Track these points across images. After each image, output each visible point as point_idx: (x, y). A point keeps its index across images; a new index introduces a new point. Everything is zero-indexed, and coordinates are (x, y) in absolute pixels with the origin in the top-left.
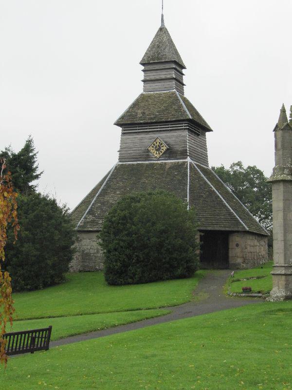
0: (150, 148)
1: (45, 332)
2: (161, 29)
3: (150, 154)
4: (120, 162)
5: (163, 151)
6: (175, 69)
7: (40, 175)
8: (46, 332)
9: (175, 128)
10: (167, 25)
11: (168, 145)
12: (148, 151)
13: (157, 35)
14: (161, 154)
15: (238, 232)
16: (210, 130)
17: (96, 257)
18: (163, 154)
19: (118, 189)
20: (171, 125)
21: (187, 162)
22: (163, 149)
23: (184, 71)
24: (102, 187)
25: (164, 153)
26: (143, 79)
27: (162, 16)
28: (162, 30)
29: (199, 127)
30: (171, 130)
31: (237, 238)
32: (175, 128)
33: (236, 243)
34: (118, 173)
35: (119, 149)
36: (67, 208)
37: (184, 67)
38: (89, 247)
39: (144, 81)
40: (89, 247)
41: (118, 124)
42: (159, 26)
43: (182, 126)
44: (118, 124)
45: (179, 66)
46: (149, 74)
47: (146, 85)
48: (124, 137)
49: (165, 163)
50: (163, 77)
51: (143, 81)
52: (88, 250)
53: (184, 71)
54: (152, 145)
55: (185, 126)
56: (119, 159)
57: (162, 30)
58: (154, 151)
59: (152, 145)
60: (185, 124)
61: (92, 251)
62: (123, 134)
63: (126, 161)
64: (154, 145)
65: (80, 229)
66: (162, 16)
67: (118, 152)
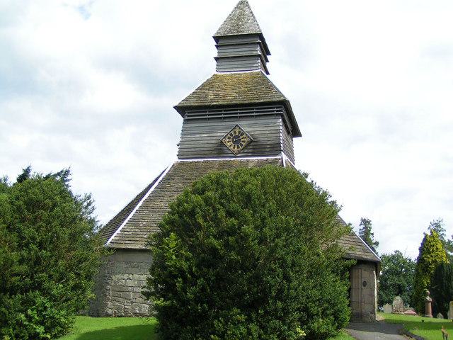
3: (225, 148)
4: (179, 159)
5: (244, 144)
6: (259, 43)
12: (222, 144)
13: (237, 7)
16: (27, 171)
18: (243, 148)
23: (268, 57)
24: (161, 179)
25: (246, 147)
26: (216, 55)
29: (294, 131)
30: (240, 117)
33: (363, 280)
34: (174, 174)
35: (178, 140)
37: (269, 53)
39: (216, 59)
41: (181, 109)
43: (273, 111)
44: (181, 109)
45: (266, 51)
49: (248, 161)
51: (216, 59)
53: (268, 57)
62: (186, 121)
63: (187, 159)
64: (231, 135)
65: (115, 246)
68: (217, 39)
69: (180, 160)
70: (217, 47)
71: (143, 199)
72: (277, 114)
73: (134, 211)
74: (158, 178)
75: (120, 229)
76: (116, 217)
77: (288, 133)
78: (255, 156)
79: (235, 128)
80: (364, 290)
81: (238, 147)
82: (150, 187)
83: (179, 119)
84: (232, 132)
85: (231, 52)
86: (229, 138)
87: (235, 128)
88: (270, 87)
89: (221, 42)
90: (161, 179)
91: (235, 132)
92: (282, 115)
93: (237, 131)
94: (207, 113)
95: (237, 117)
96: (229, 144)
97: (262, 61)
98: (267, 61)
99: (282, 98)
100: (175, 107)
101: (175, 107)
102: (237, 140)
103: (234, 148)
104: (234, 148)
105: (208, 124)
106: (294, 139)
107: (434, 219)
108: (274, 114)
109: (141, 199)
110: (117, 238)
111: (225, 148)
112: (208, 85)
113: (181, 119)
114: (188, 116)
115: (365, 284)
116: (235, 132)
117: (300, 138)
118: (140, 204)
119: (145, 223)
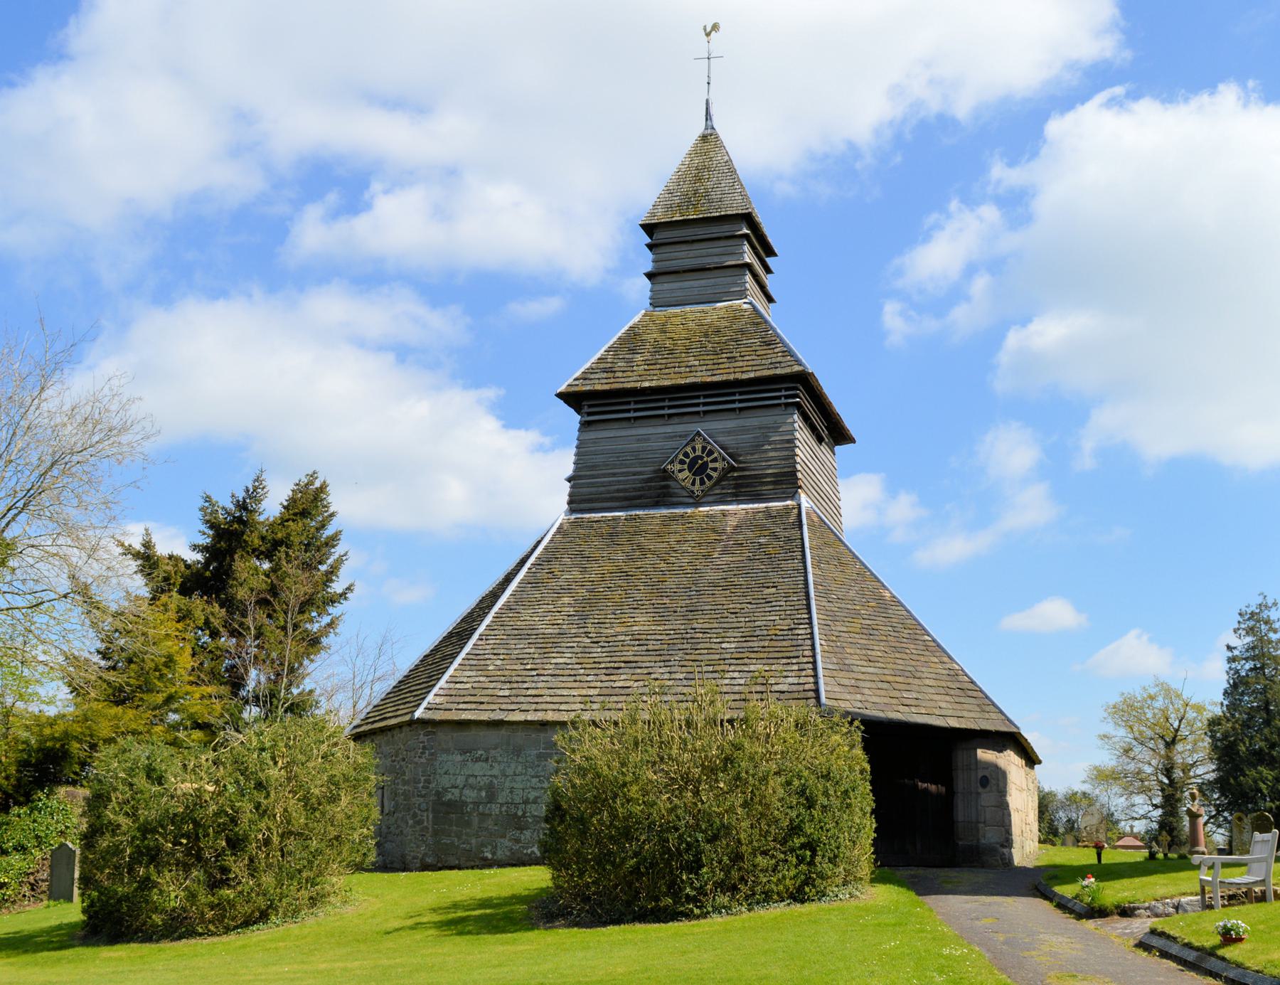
1: (806, 616)
2: (704, 138)
3: (671, 483)
6: (746, 236)
7: (340, 616)
8: (807, 624)
12: (665, 475)
17: (483, 816)
19: (568, 590)
22: (715, 469)
23: (770, 261)
26: (649, 267)
27: (707, 101)
28: (709, 138)
30: (705, 412)
33: (980, 774)
36: (317, 484)
37: (770, 252)
38: (460, 781)
39: (650, 276)
40: (460, 781)
42: (700, 128)
44: (572, 398)
46: (667, 252)
47: (658, 287)
48: (592, 435)
49: (724, 514)
50: (565, 694)
52: (456, 792)
53: (770, 261)
54: (681, 457)
56: (570, 503)
57: (709, 138)
59: (681, 457)
61: (470, 795)
62: (585, 425)
64: (686, 455)
65: (438, 716)
66: (707, 101)
67: (569, 480)
68: (649, 228)
69: (573, 517)
71: (496, 609)
72: (787, 405)
73: (476, 636)
74: (494, 595)
75: (446, 677)
76: (435, 650)
77: (820, 440)
78: (740, 502)
79: (693, 440)
80: (984, 796)
81: (702, 483)
82: (508, 579)
83: (572, 419)
84: (689, 449)
85: (684, 257)
86: (682, 462)
87: (693, 440)
88: (771, 341)
89: (661, 236)
90: (532, 560)
91: (694, 449)
93: (699, 447)
94: (632, 406)
95: (698, 413)
96: (681, 476)
97: (755, 276)
98: (768, 270)
99: (797, 368)
102: (698, 468)
103: (693, 484)
104: (693, 484)
105: (633, 432)
106: (837, 448)
107: (1043, 762)
108: (779, 405)
109: (490, 607)
110: (438, 700)
112: (631, 341)
117: (851, 445)
118: (488, 620)
119: (499, 663)
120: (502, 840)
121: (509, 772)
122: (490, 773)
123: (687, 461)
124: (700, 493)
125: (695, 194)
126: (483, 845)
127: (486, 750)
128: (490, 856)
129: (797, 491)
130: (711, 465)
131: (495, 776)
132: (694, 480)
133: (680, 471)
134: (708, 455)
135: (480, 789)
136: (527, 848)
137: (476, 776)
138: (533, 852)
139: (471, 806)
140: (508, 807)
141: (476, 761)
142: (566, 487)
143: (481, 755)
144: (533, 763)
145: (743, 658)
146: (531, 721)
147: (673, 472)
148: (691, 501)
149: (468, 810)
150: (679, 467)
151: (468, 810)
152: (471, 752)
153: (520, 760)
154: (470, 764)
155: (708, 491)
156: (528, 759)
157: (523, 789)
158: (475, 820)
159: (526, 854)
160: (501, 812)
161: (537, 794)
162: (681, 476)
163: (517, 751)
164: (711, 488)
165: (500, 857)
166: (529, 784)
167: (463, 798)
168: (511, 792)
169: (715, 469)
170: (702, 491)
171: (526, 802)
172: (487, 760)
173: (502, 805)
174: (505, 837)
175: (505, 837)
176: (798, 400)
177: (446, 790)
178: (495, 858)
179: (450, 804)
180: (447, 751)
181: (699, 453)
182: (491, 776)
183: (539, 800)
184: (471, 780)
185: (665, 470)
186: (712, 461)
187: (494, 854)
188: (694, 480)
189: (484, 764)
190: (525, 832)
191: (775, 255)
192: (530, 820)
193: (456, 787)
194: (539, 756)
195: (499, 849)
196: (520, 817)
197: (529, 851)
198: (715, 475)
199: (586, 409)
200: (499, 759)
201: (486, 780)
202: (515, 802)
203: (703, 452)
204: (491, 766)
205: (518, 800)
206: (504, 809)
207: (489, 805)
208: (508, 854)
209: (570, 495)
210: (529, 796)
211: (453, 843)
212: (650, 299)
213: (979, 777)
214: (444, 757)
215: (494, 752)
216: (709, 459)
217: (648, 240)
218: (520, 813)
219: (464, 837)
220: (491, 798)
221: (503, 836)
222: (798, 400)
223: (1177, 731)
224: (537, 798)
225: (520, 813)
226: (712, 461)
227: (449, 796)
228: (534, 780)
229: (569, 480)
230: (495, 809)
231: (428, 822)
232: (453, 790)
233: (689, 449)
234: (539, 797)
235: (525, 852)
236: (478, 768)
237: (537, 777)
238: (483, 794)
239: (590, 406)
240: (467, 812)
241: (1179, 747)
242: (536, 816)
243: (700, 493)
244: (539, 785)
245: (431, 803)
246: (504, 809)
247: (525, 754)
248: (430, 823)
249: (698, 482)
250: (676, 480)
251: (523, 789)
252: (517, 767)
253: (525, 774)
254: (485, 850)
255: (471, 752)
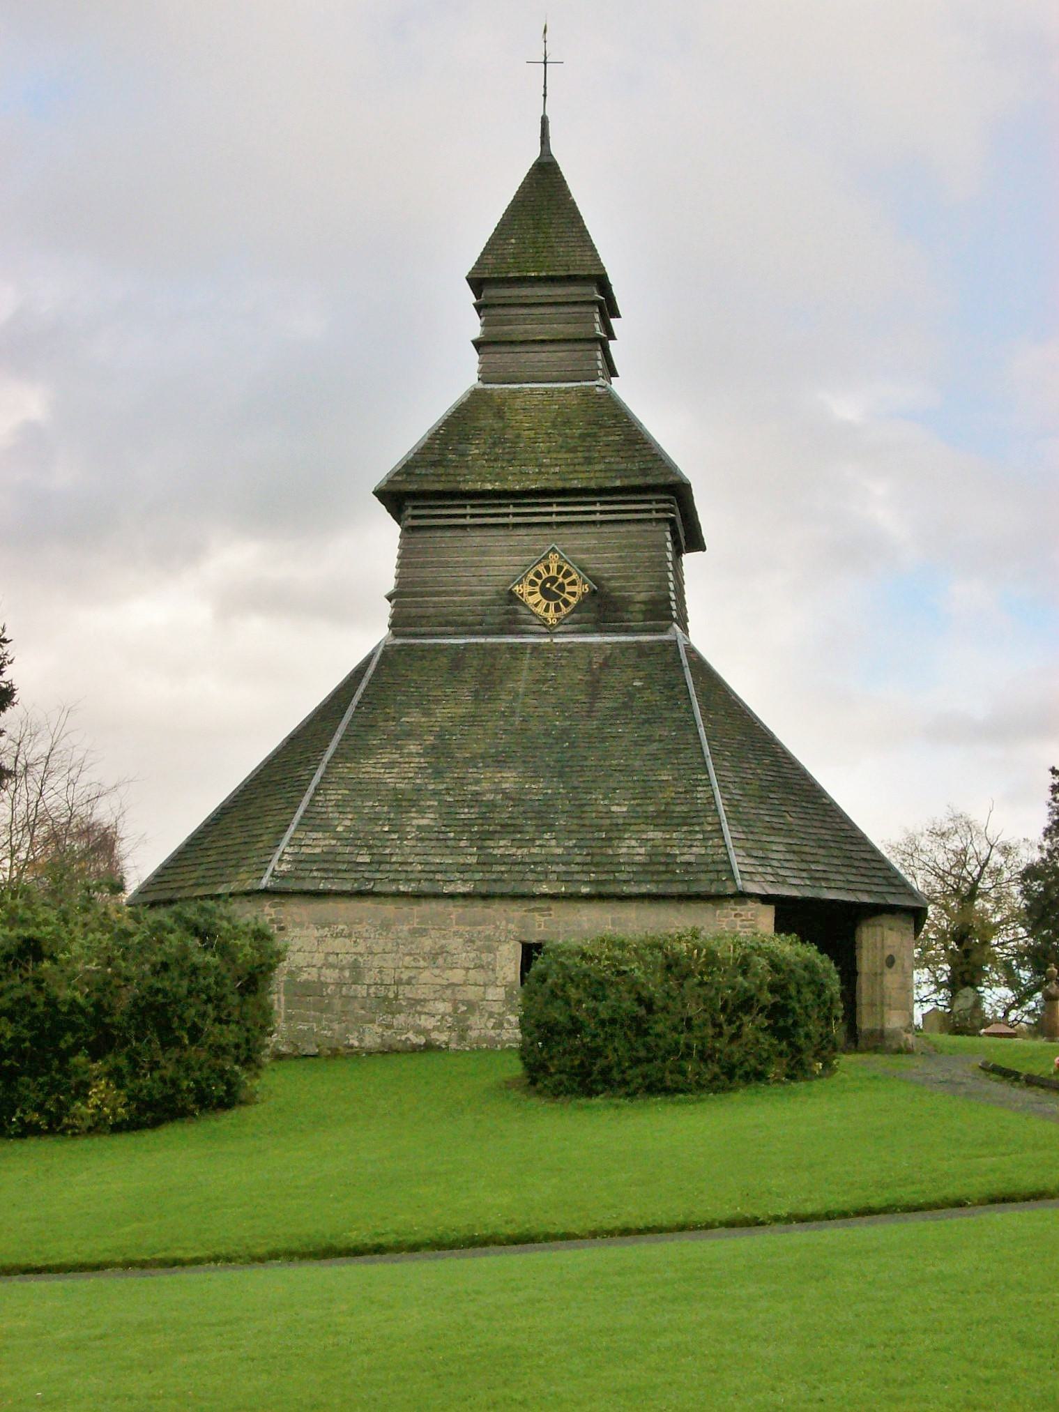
0: (522, 589)
3: (520, 608)
9: (629, 516)
10: (558, 152)
11: (594, 579)
12: (513, 598)
14: (565, 610)
15: (892, 910)
18: (573, 612)
20: (559, 504)
21: (674, 643)
22: (573, 594)
23: (613, 321)
27: (544, 122)
30: (516, 525)
31: (887, 933)
32: (629, 516)
33: (887, 953)
35: (390, 585)
38: (318, 959)
39: (478, 344)
43: (507, 515)
45: (609, 309)
51: (478, 344)
53: (613, 321)
54: (531, 576)
55: (658, 511)
58: (538, 597)
60: (658, 502)
61: (330, 975)
62: (408, 531)
64: (538, 575)
66: (544, 122)
67: (389, 598)
69: (399, 641)
70: (479, 308)
81: (557, 609)
84: (541, 568)
86: (533, 583)
87: (546, 557)
89: (490, 293)
91: (547, 568)
92: (672, 522)
93: (554, 566)
100: (618, 376)
101: (618, 376)
103: (547, 610)
104: (547, 610)
111: (520, 608)
113: (396, 529)
114: (414, 517)
115: (890, 962)
116: (547, 568)
120: (370, 1025)
121: (377, 949)
122: (353, 950)
123: (539, 582)
124: (555, 622)
125: (534, 243)
126: (347, 1030)
127: (350, 924)
128: (356, 1044)
129: (671, 625)
130: (568, 589)
131: (361, 955)
132: (548, 606)
133: (531, 594)
134: (565, 576)
135: (342, 969)
136: (401, 1034)
137: (337, 954)
138: (408, 1039)
139: (332, 987)
140: (377, 989)
141: (336, 937)
142: (387, 609)
143: (343, 930)
144: (406, 940)
145: (640, 824)
146: (403, 892)
147: (522, 595)
148: (544, 630)
149: (329, 991)
150: (529, 589)
151: (329, 991)
152: (329, 927)
153: (390, 935)
154: (329, 940)
155: (564, 619)
156: (400, 934)
157: (395, 969)
158: (337, 1002)
159: (400, 1041)
160: (368, 994)
161: (411, 975)
162: (532, 600)
163: (386, 926)
164: (566, 616)
165: (368, 1044)
166: (401, 963)
167: (322, 979)
168: (380, 972)
169: (573, 594)
170: (558, 619)
171: (398, 982)
172: (350, 936)
173: (369, 986)
174: (375, 1023)
175: (375, 1023)
176: (672, 515)
177: (300, 969)
178: (363, 1045)
179: (306, 984)
180: (300, 925)
181: (553, 573)
182: (355, 953)
183: (414, 981)
184: (332, 959)
185: (511, 593)
186: (570, 584)
187: (361, 1040)
188: (548, 606)
189: (347, 940)
190: (398, 1016)
191: (619, 316)
192: (404, 1003)
193: (314, 966)
194: (413, 932)
195: (367, 1035)
196: (392, 999)
197: (403, 1038)
198: (573, 600)
199: (410, 511)
200: (365, 935)
201: (350, 958)
202: (385, 983)
203: (559, 573)
204: (355, 942)
205: (388, 981)
206: (372, 990)
207: (353, 986)
208: (379, 1040)
209: (392, 617)
210: (402, 976)
211: (311, 1029)
212: (479, 373)
213: (885, 958)
214: (297, 931)
215: (358, 926)
216: (566, 581)
217: (474, 300)
218: (391, 995)
219: (324, 1023)
220: (357, 978)
221: (372, 1021)
222: (672, 515)
223: (976, 882)
224: (411, 978)
225: (391, 995)
226: (570, 584)
227: (304, 977)
228: (407, 958)
229: (389, 598)
230: (361, 991)
231: (279, 1007)
232: (309, 970)
233: (541, 568)
234: (415, 978)
235: (398, 1038)
236: (338, 944)
237: (410, 954)
238: (347, 974)
239: (415, 507)
240: (328, 994)
241: (979, 903)
242: (409, 999)
243: (555, 622)
244: (413, 964)
245: (282, 984)
246: (372, 990)
247: (396, 929)
248: (283, 1007)
249: (552, 608)
250: (524, 605)
251: (395, 969)
252: (386, 945)
253: (397, 952)
254: (351, 1036)
255: (329, 927)
